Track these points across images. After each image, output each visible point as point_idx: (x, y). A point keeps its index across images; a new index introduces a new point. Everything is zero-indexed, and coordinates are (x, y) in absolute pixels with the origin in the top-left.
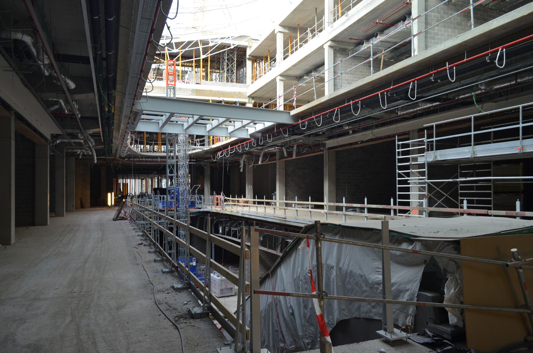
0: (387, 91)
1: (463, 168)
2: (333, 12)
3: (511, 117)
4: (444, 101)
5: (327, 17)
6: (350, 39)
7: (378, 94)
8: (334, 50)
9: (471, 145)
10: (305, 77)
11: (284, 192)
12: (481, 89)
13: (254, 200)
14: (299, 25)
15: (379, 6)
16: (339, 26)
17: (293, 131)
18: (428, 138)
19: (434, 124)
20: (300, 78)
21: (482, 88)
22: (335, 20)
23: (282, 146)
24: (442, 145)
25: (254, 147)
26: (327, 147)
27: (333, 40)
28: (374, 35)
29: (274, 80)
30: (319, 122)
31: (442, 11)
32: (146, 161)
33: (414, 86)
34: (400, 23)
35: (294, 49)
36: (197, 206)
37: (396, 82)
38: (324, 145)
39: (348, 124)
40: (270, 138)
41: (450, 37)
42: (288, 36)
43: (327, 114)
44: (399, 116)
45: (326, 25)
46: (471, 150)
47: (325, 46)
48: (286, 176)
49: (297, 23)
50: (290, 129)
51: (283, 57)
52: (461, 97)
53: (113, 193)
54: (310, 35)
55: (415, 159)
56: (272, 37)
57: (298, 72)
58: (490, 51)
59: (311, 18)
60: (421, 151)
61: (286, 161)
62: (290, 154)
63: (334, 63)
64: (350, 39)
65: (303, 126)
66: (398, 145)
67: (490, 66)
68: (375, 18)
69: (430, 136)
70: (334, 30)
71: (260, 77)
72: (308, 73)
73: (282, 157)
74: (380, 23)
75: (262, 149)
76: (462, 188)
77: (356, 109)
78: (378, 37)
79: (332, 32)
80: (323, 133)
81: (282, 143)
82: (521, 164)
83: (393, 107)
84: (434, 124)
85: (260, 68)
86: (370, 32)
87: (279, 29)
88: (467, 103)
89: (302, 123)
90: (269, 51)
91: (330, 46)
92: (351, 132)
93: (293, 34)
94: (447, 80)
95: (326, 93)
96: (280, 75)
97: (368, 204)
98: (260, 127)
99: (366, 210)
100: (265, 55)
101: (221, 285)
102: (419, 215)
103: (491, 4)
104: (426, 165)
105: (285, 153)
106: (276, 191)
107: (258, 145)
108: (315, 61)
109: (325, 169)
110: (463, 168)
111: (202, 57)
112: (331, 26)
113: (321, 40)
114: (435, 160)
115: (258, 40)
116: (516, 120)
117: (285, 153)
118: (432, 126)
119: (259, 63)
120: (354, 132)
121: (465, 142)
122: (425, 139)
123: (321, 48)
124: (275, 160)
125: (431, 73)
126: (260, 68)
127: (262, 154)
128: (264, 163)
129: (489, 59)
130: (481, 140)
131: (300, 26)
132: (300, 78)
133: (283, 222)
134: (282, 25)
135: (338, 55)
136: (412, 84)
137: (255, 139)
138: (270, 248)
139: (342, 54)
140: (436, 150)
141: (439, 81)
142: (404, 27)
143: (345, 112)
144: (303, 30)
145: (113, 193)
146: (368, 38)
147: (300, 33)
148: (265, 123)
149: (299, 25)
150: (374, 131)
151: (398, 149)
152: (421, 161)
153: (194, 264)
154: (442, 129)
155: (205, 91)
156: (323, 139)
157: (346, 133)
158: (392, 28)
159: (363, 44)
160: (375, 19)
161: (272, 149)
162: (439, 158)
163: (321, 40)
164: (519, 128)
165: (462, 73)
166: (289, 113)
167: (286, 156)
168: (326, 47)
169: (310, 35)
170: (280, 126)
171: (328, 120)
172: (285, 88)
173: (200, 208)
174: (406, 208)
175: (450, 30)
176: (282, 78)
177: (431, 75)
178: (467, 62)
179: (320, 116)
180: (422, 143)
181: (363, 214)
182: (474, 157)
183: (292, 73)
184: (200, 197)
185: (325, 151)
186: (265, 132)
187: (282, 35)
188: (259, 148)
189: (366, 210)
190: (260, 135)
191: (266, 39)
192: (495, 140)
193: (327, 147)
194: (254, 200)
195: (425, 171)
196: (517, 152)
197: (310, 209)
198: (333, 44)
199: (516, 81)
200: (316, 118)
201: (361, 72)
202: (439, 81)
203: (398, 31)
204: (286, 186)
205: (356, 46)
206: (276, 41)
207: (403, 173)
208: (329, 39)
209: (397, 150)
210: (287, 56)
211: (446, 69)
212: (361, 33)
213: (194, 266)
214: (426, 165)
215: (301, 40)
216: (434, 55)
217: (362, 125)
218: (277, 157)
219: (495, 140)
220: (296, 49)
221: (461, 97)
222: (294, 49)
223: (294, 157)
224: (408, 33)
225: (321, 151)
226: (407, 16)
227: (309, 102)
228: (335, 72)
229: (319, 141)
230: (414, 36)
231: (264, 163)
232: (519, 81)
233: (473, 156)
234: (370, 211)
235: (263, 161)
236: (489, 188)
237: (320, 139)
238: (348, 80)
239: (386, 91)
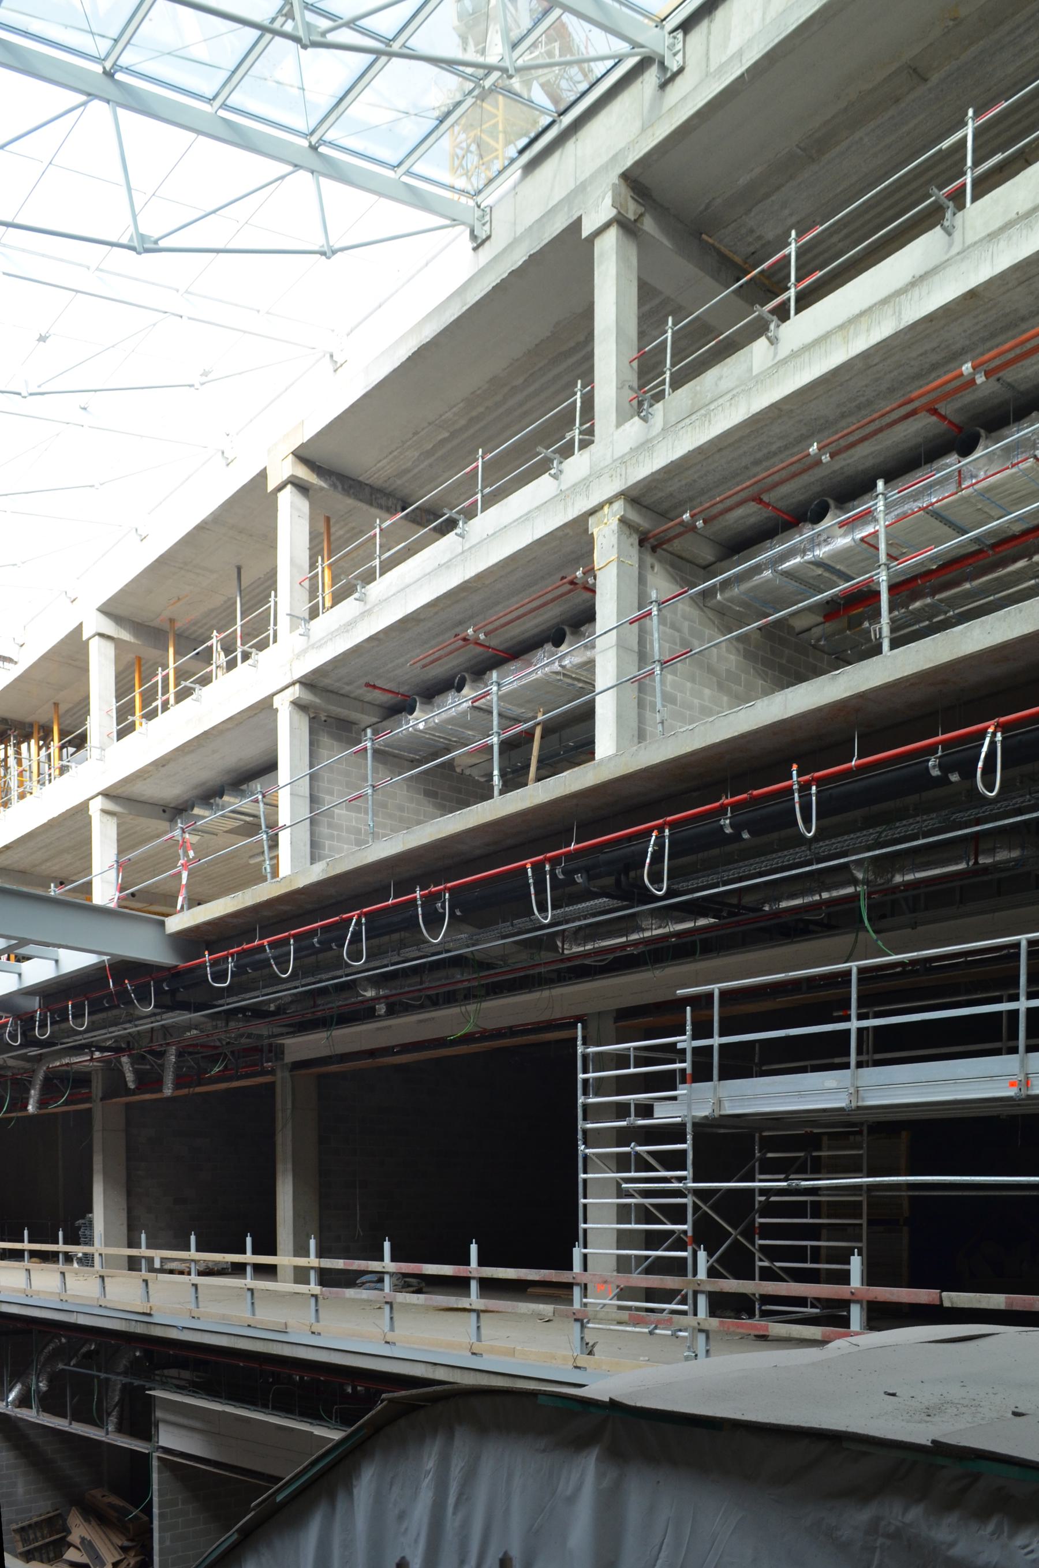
0: (555, 862)
1: (769, 1144)
2: (306, 584)
3: (824, 998)
4: (731, 914)
5: (287, 597)
6: (368, 685)
7: (524, 868)
8: (312, 720)
9: (846, 1066)
10: (197, 811)
12: (855, 882)
13: (302, 1262)
14: (172, 621)
15: (479, 577)
16: (333, 635)
17: (173, 992)
18: (694, 1037)
19: (716, 988)
20: (176, 811)
21: (860, 876)
22: (314, 613)
23: (117, 1050)
24: (740, 1064)
25: (10, 1048)
26: (290, 1058)
27: (308, 682)
28: (452, 684)
29: (81, 812)
30: (282, 962)
31: (686, 624)
33: (660, 843)
34: (540, 653)
35: (158, 703)
37: (589, 827)
38: (279, 1052)
39: (378, 981)
40: (78, 1015)
41: (408, 824)
42: (130, 657)
43: (313, 933)
44: (570, 959)
45: (283, 623)
46: (847, 1083)
47: (277, 702)
48: (128, 1159)
49: (167, 614)
50: (171, 984)
51: (114, 729)
52: (784, 904)
54: (220, 658)
55: (646, 1110)
56: (71, 653)
57: (171, 791)
58: (941, 737)
59: (218, 600)
60: (668, 1081)
61: (128, 1106)
62: (149, 1081)
63: (311, 766)
64: (368, 685)
65: (220, 976)
66: (585, 1057)
67: (728, 848)
68: (462, 623)
69: (702, 1030)
70: (313, 647)
71: (22, 796)
72: (210, 796)
73: (115, 1087)
74: (477, 643)
75: (39, 1058)
76: (769, 1209)
77: (434, 921)
78: (465, 691)
79: (305, 651)
80: (280, 1010)
81: (117, 1039)
82: (904, 1134)
83: (594, 915)
84: (716, 988)
85: (19, 762)
86: (438, 671)
87: (94, 623)
88: (838, 919)
89: (214, 963)
90: (56, 705)
91: (298, 705)
92: (381, 1009)
93: (150, 653)
94: (789, 831)
95: (605, 744)
96: (106, 794)
97: (481, 1264)
98: (38, 971)
99: (474, 1285)
100: (42, 715)
102: (296, 1282)
103: (817, 631)
104: (689, 1129)
105: (130, 1077)
106: (90, 1210)
107: (29, 1041)
108: (241, 753)
109: (279, 1139)
110: (769, 1144)
112: (301, 630)
113: (268, 675)
114: (716, 1114)
115: (10, 660)
116: (838, 1010)
117: (130, 1077)
118: (710, 995)
119: (17, 745)
120: (393, 1010)
121: (826, 1054)
122: (684, 1041)
123: (265, 708)
124: (88, 1099)
125: (724, 801)
126: (19, 762)
127: (40, 1076)
128: (51, 1109)
129: (563, 873)
130: (890, 1047)
131: (179, 625)
132: (176, 811)
133: (140, 1329)
134: (107, 610)
135: (325, 739)
136: (657, 839)
137: (17, 1017)
138: (77, 1417)
139: (339, 739)
140: (721, 1078)
141: (746, 836)
142: (556, 667)
143: (393, 928)
144: (191, 641)
146: (433, 692)
147: (178, 654)
148: (62, 952)
149: (172, 621)
150: (485, 1005)
151: (585, 1071)
152: (665, 1114)
154: (744, 1009)
156: (277, 1030)
157: (365, 1013)
158: (512, 666)
159: (411, 712)
160: (460, 623)
161: (80, 1060)
162: (730, 1109)
163: (268, 675)
164: (848, 1031)
165: (840, 807)
166: (162, 924)
167: (132, 1086)
168: (283, 704)
169: (220, 658)
170: (124, 969)
171: (317, 956)
172: (125, 843)
174: (669, 1282)
175: (707, 692)
176: (110, 806)
177: (722, 811)
178: (860, 768)
179: (285, 942)
180: (674, 1053)
181: (463, 1302)
182: (858, 1108)
183: (149, 790)
185: (279, 1074)
186: (57, 993)
187: (109, 649)
188: (33, 1052)
189: (474, 1285)
190: (35, 1003)
191: (44, 658)
192: (878, 1056)
193: (290, 1058)
194: (302, 1262)
195: (685, 1151)
196: (1011, 1092)
197: (194, 1278)
198: (308, 697)
199: (976, 862)
200: (272, 945)
201: (401, 809)
202: (746, 836)
203: (534, 677)
204: (129, 1194)
205: (385, 718)
206: (85, 670)
207: (649, 1153)
208: (298, 674)
209: (581, 1076)
210: (130, 728)
211: (789, 790)
212: (408, 668)
214: (689, 1129)
215: (181, 674)
216: (742, 736)
217: (433, 983)
218: (97, 1088)
219: (878, 1056)
220: (165, 706)
221: (784, 904)
222: (158, 703)
223: (168, 1091)
224: (582, 681)
225: (264, 1073)
226: (567, 630)
227: (199, 904)
228: (314, 800)
229: (260, 1037)
230: (284, 827)
231: (51, 1109)
232: (984, 860)
233: (854, 1105)
234: (489, 1286)
235: (42, 1103)
236: (853, 1209)
237: (265, 1032)
238: (358, 832)
239: (550, 860)
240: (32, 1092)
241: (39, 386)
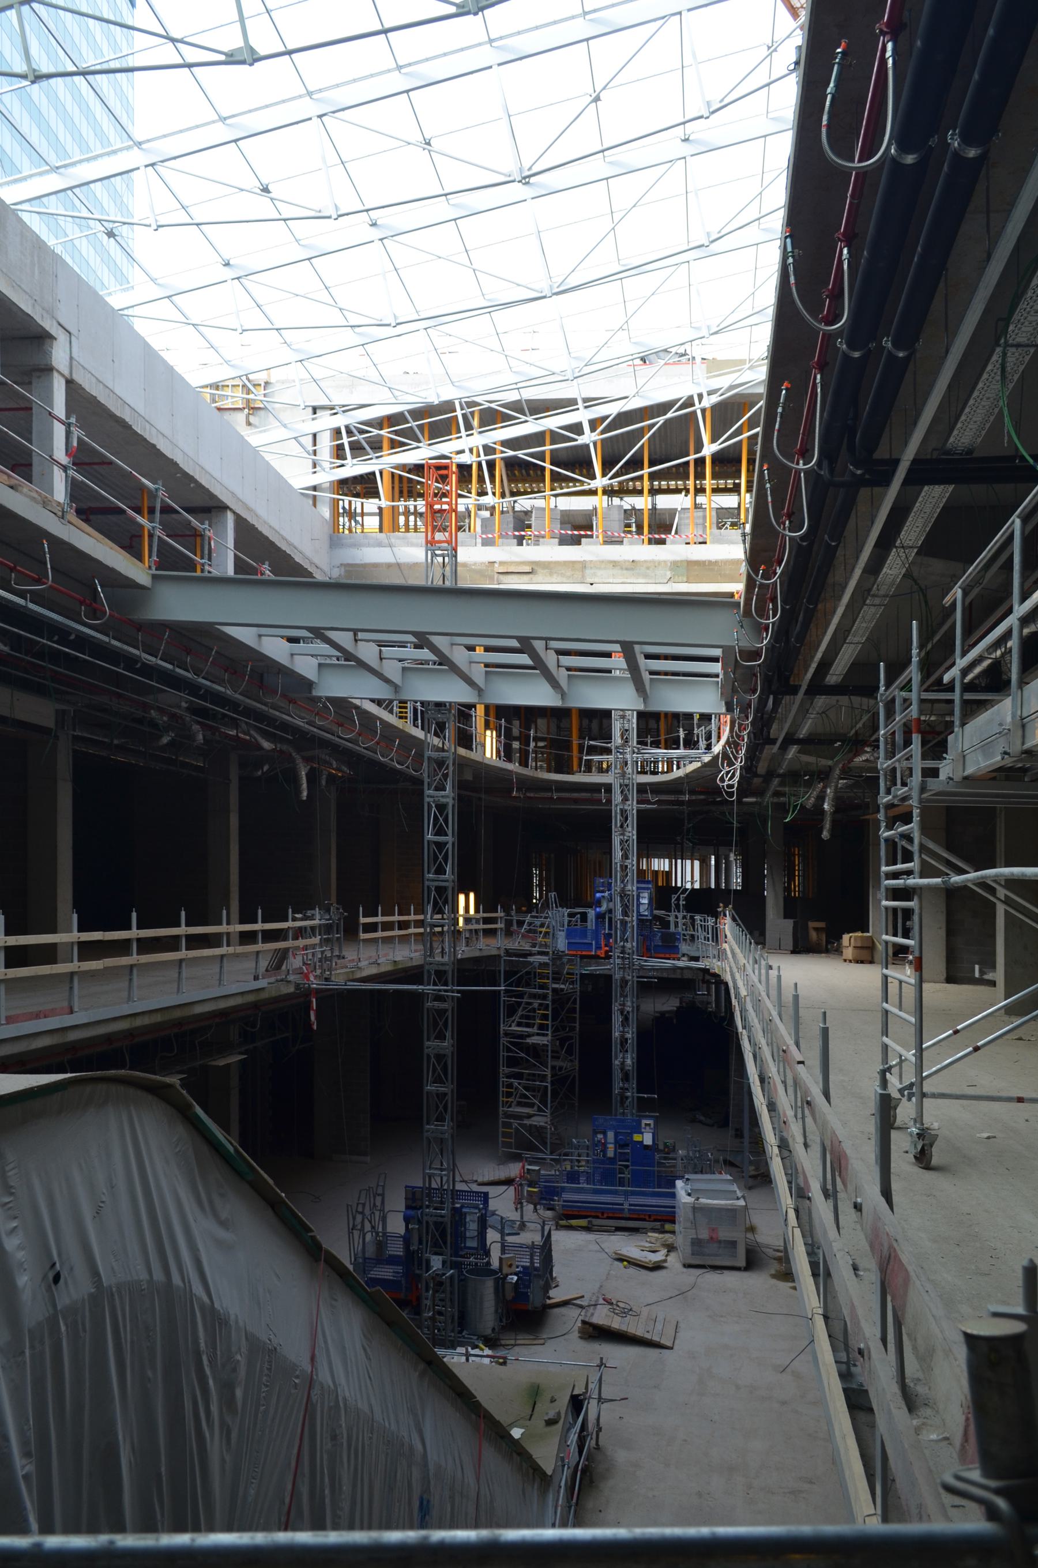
11: (942, 918)
32: (576, 801)
36: (684, 948)
53: (472, 896)
101: (694, 1224)
111: (709, 449)
145: (472, 896)
153: (648, 1139)
155: (716, 562)
173: (696, 959)
184: (692, 918)
213: (647, 1147)
240: (829, 791)
241: (721, 101)
